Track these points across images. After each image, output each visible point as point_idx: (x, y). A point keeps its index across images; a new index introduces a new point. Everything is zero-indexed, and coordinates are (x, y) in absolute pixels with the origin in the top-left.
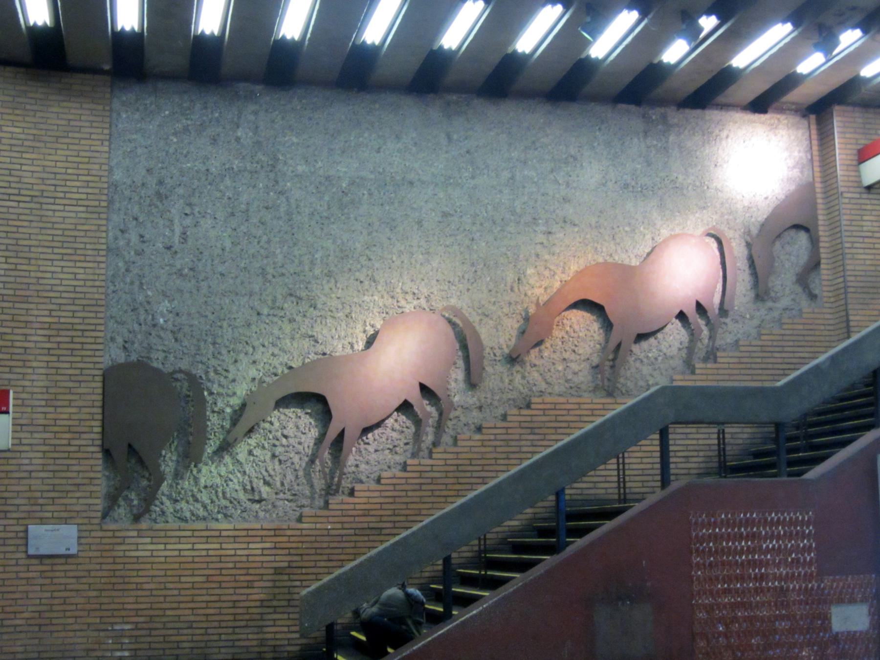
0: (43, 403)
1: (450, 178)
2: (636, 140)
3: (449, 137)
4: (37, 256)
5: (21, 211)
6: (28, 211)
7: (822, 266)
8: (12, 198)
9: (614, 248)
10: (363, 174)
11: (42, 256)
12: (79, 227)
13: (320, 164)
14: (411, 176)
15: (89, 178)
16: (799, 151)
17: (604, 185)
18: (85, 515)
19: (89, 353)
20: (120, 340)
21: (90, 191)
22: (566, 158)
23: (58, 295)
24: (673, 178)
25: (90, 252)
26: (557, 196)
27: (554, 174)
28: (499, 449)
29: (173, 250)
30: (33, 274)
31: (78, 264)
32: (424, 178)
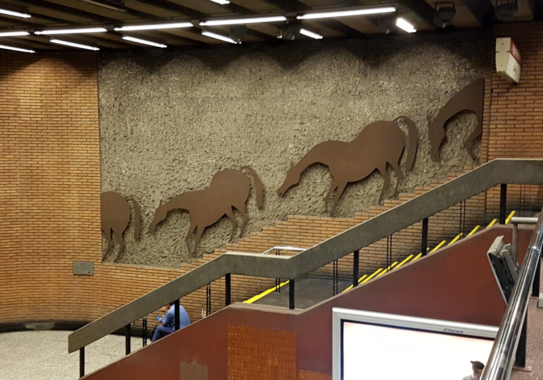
0: (78, 209)
1: (251, 94)
2: (358, 62)
3: (251, 71)
4: (71, 143)
5: (62, 122)
6: (66, 122)
7: (483, 138)
8: (59, 116)
9: (339, 131)
10: (209, 95)
11: (73, 143)
12: (88, 128)
13: (188, 92)
14: (231, 95)
15: (90, 105)
16: (437, 65)
17: (336, 92)
18: (96, 258)
19: (95, 187)
20: (108, 180)
21: (91, 111)
22: (315, 78)
23: (81, 160)
24: (380, 84)
25: (92, 140)
26: (309, 101)
27: (307, 88)
28: (270, 241)
29: (127, 137)
30: (70, 151)
31: (88, 146)
32: (237, 96)
